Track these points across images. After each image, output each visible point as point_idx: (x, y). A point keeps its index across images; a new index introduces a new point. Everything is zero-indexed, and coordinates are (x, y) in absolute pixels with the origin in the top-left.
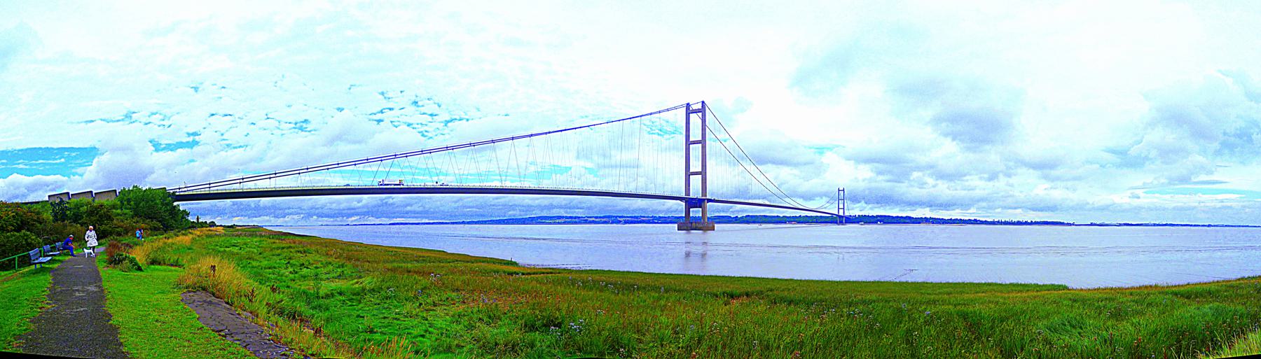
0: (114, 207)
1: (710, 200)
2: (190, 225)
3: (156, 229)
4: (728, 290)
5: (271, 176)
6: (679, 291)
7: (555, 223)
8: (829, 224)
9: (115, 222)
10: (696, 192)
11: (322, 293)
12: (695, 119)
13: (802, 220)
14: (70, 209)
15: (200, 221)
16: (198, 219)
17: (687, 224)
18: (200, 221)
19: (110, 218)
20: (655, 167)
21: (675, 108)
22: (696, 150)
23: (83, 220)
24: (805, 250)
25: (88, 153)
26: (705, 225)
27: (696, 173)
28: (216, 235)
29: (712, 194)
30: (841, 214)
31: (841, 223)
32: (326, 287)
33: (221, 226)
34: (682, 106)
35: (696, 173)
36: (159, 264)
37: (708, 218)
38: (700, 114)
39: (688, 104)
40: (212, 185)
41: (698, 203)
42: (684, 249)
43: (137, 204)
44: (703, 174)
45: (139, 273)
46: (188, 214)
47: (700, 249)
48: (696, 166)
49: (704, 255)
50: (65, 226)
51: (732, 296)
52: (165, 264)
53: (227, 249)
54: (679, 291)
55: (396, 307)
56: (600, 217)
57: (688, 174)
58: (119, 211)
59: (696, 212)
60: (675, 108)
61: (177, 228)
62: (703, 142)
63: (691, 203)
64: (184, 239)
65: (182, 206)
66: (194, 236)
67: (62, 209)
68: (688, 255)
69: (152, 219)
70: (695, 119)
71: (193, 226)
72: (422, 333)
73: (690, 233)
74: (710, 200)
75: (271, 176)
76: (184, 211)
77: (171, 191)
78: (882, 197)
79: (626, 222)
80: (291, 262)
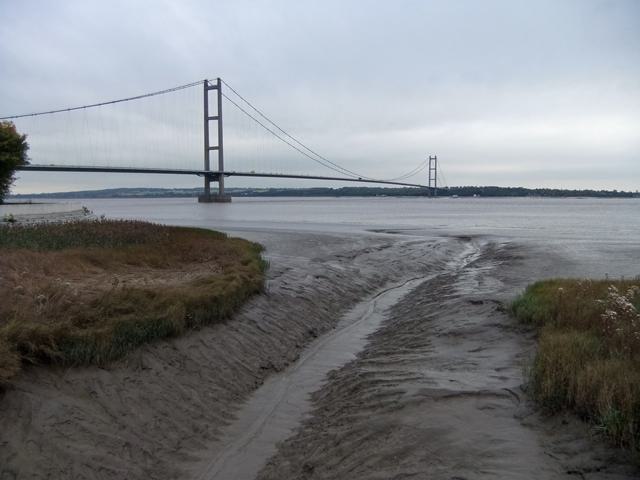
1: (229, 174)
8: (421, 199)
10: (214, 167)
12: (213, 94)
17: (206, 197)
20: (199, 182)
22: (213, 125)
26: (222, 197)
30: (433, 186)
34: (198, 83)
39: (206, 82)
44: (220, 148)
48: (214, 142)
57: (207, 149)
59: (214, 185)
60: (193, 85)
63: (210, 176)
70: (213, 94)
74: (229, 174)
78: (95, 304)
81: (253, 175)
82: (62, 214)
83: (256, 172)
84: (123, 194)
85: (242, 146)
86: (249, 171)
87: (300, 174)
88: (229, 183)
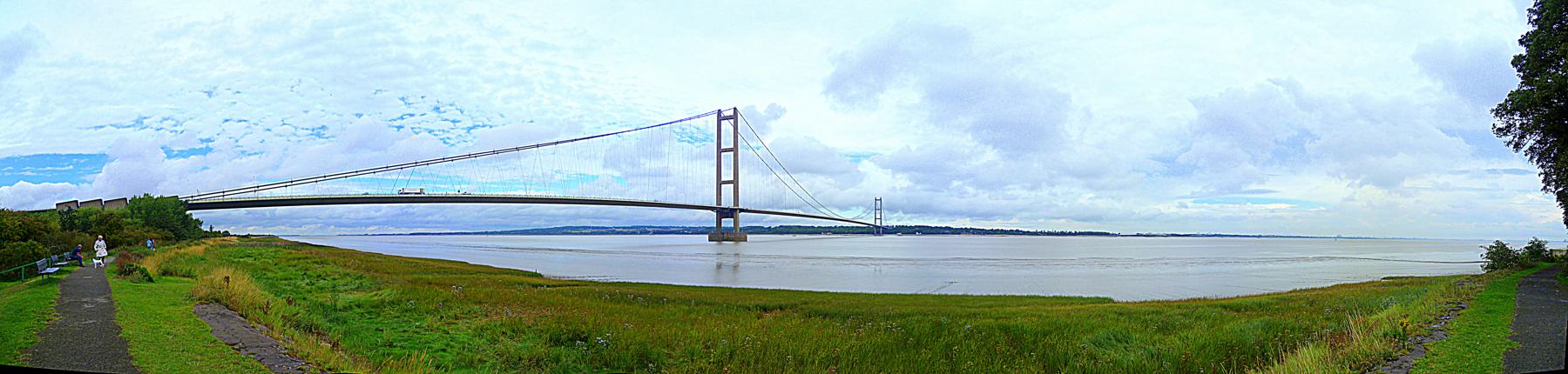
0: (124, 216)
2: (203, 234)
3: (167, 239)
4: (761, 303)
5: (288, 184)
6: (710, 304)
7: (581, 234)
9: (125, 231)
10: (727, 202)
11: (339, 305)
12: (727, 126)
13: (837, 230)
14: (78, 218)
15: (213, 230)
16: (211, 228)
17: (718, 235)
18: (213, 230)
19: (120, 227)
21: (706, 115)
22: (727, 158)
23: (93, 230)
24: (841, 262)
25: (97, 160)
26: (737, 235)
27: (726, 150)
28: (230, 245)
29: (745, 204)
30: (878, 224)
31: (878, 233)
32: (344, 299)
33: (235, 235)
34: (713, 112)
35: (726, 150)
36: (171, 274)
37: (741, 229)
38: (732, 121)
40: (226, 193)
41: (730, 213)
42: (714, 261)
43: (148, 213)
44: (735, 182)
45: (151, 284)
46: (201, 224)
47: (732, 261)
49: (736, 267)
50: (74, 235)
51: (765, 310)
52: (176, 275)
53: (241, 260)
54: (710, 304)
55: (416, 320)
56: (628, 228)
57: (720, 183)
58: (129, 220)
59: (727, 223)
60: (706, 115)
61: (190, 238)
62: (735, 150)
63: (723, 213)
64: (197, 249)
65: (196, 214)
66: (207, 246)
67: (70, 218)
68: (719, 266)
69: (164, 228)
70: (727, 126)
71: (207, 235)
72: (444, 347)
73: (720, 244)
75: (288, 184)
76: (197, 220)
77: (184, 200)
79: (655, 233)
80: (308, 273)
81: (1274, 236)
82: (673, 220)
83: (428, 192)
84: (569, 231)
85: (755, 187)
86: (395, 193)
87: (452, 193)
88: (745, 220)
